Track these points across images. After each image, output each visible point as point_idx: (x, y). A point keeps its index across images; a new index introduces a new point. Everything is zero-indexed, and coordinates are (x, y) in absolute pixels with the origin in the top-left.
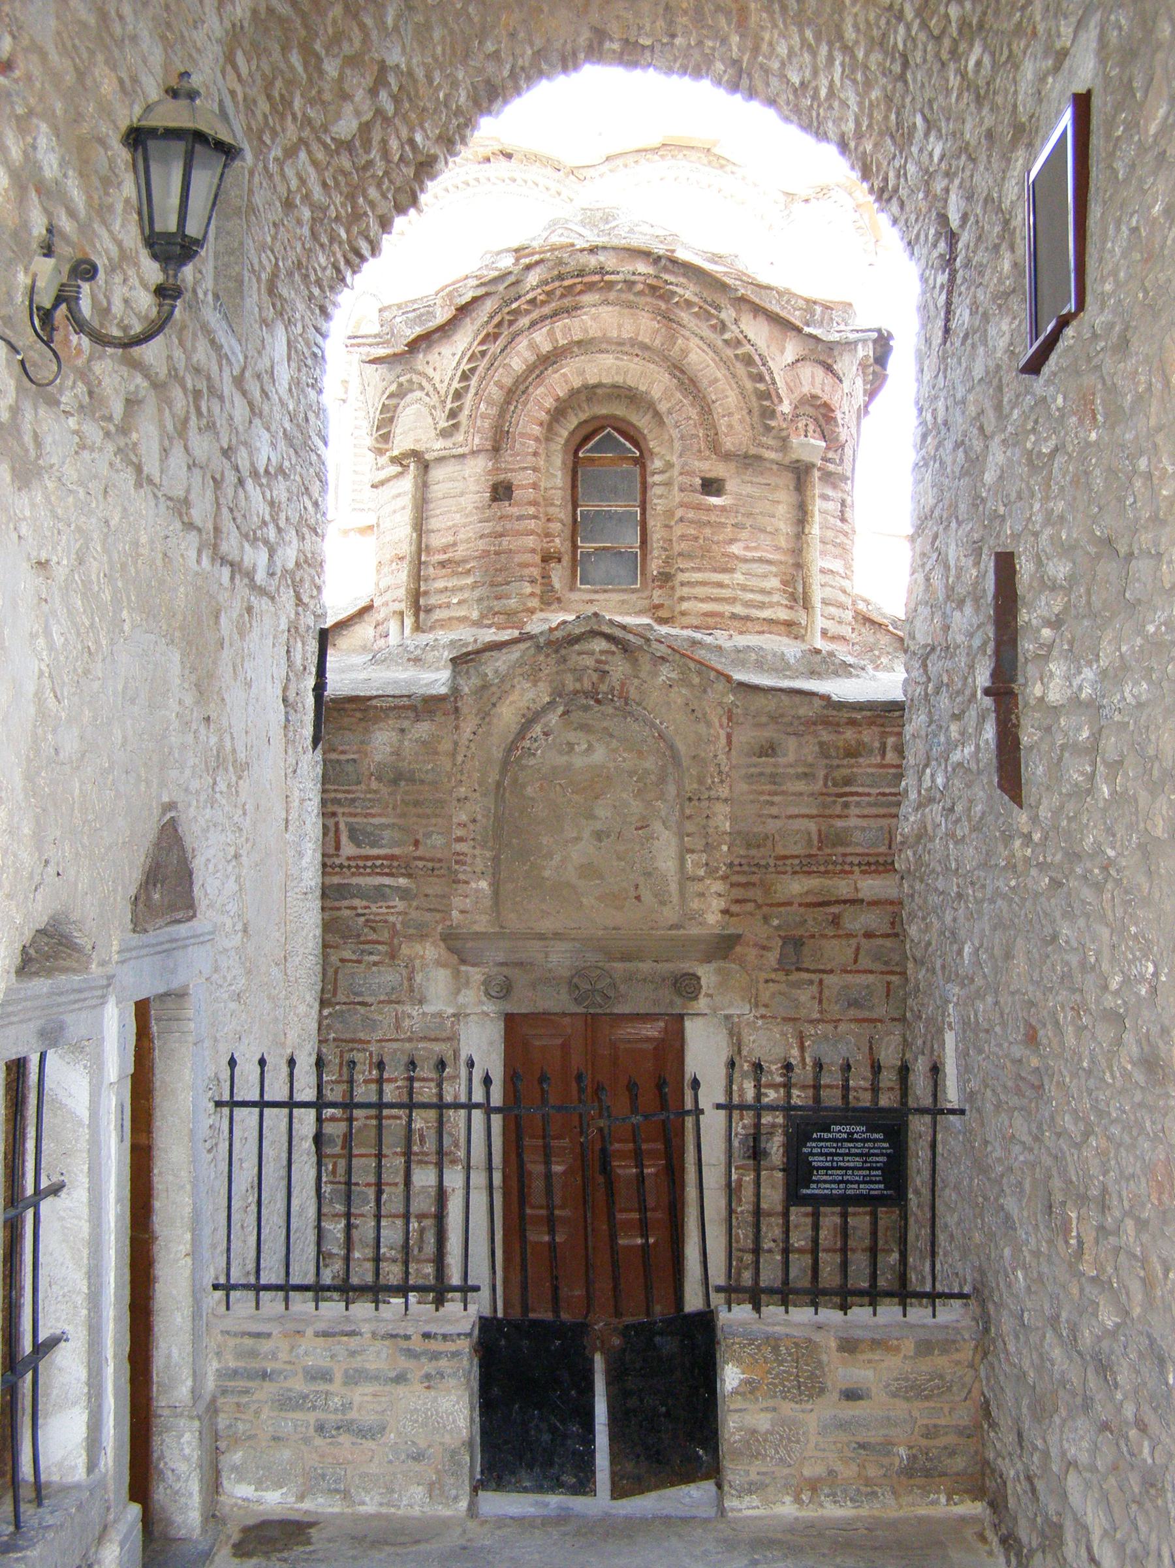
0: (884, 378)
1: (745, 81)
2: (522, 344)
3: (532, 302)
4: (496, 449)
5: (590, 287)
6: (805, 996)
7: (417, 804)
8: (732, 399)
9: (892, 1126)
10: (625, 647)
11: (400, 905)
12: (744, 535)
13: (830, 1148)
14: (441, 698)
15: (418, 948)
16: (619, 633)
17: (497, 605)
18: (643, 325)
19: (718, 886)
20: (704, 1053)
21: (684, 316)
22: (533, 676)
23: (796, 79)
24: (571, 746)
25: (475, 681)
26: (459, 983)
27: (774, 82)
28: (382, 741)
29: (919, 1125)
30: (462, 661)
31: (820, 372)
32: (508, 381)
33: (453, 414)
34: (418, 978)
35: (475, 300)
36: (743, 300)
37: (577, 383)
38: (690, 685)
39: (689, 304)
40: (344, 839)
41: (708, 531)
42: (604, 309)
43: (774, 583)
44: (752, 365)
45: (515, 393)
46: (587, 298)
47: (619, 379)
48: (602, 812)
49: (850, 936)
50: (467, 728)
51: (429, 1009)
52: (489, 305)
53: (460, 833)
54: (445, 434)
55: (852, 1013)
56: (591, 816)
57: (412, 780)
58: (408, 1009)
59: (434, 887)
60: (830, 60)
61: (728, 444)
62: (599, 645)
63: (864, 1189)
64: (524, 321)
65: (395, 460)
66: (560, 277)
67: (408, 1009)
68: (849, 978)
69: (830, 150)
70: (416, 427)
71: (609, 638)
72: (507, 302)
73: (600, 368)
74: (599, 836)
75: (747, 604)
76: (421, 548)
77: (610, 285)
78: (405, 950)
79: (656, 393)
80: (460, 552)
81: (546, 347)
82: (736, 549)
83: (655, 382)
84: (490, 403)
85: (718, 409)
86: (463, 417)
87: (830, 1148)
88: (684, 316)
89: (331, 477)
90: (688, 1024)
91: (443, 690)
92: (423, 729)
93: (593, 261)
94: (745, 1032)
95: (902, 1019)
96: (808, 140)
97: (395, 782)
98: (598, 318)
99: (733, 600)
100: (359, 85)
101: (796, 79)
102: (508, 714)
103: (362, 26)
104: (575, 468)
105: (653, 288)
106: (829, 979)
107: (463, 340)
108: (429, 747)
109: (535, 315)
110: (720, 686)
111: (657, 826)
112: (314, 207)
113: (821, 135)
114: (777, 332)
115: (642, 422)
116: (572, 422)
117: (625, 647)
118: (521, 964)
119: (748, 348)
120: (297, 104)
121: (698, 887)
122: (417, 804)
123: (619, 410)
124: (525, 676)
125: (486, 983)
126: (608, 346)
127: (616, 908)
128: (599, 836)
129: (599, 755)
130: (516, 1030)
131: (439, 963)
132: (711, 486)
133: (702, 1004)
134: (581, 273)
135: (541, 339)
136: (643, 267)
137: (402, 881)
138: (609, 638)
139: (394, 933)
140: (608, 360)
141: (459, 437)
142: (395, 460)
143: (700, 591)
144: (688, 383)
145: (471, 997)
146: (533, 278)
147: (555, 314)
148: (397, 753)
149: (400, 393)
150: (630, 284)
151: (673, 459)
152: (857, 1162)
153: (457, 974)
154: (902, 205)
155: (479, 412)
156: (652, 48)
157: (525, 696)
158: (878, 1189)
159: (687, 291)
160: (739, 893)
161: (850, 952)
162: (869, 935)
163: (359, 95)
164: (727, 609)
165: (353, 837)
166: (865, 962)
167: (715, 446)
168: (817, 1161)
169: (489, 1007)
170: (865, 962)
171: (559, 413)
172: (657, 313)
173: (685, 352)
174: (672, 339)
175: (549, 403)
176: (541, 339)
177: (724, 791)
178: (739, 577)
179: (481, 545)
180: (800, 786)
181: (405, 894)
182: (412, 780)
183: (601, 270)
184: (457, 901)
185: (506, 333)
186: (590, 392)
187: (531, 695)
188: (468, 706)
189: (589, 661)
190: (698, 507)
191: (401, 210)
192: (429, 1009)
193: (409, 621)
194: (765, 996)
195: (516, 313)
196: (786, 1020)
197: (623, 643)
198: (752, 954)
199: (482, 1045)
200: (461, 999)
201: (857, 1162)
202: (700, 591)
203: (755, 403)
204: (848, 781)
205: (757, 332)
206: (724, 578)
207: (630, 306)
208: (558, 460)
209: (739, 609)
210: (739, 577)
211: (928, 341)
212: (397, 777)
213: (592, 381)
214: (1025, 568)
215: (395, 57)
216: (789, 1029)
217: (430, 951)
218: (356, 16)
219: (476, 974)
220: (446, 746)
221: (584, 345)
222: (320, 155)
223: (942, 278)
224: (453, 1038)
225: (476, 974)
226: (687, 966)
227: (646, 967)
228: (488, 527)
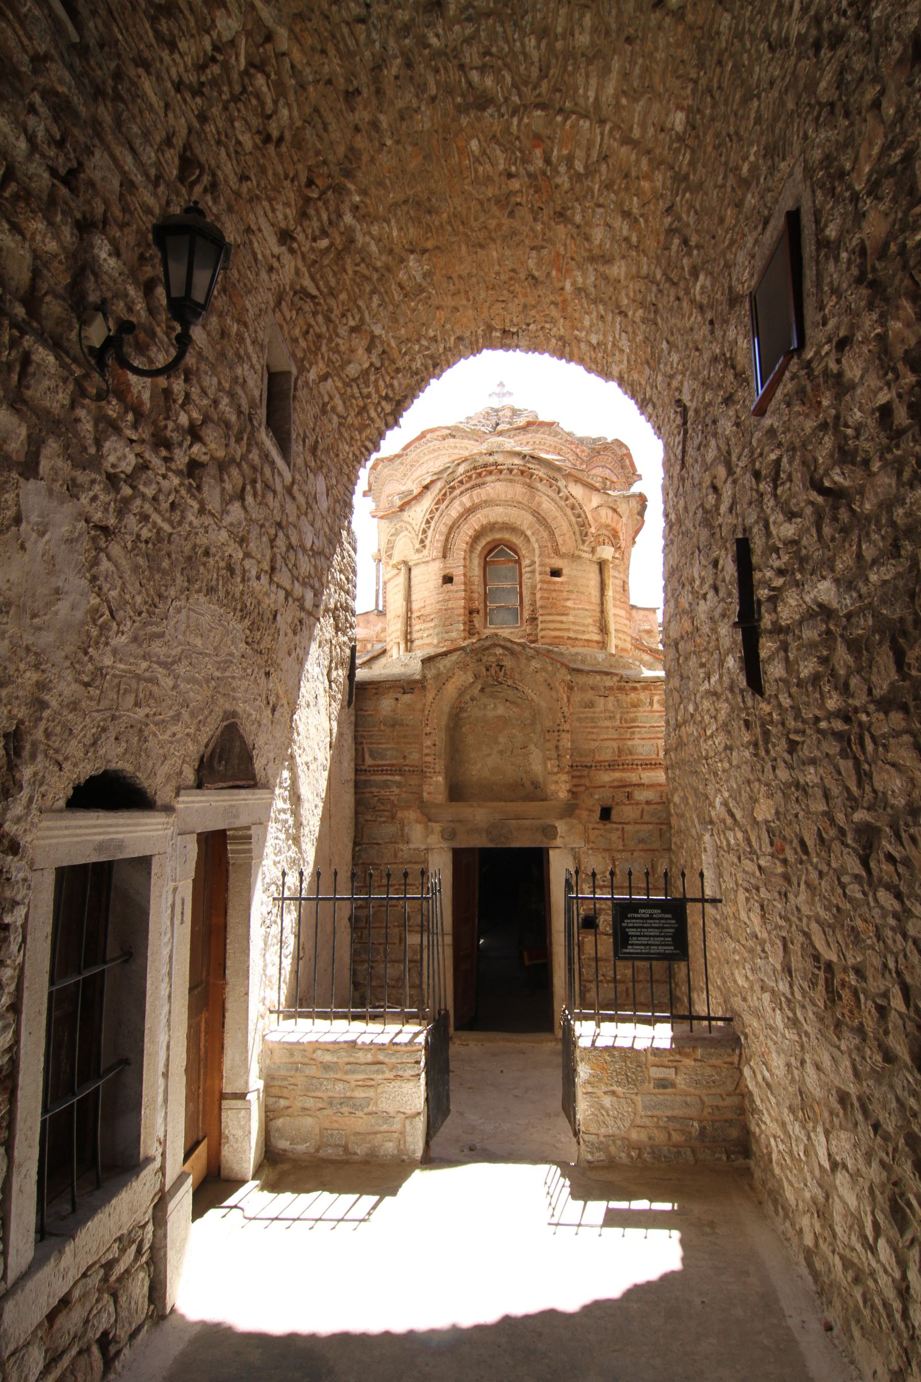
0: (643, 522)
1: (567, 349)
2: (456, 503)
3: (461, 482)
4: (444, 557)
5: (490, 473)
6: (614, 836)
7: (405, 737)
8: (565, 526)
9: (676, 909)
10: (512, 653)
11: (395, 790)
12: (574, 596)
13: (638, 923)
14: (416, 681)
15: (406, 813)
16: (509, 645)
17: (446, 636)
18: (518, 491)
19: (565, 777)
20: (559, 866)
21: (539, 485)
22: (464, 667)
23: (594, 342)
24: (485, 706)
25: (434, 671)
26: (428, 832)
27: (583, 345)
28: (386, 705)
29: (693, 910)
30: (427, 661)
31: (610, 513)
32: (450, 523)
33: (422, 541)
34: (406, 829)
35: (432, 482)
36: (569, 475)
37: (485, 522)
38: (546, 671)
39: (541, 480)
40: (367, 756)
41: (554, 595)
42: (498, 484)
43: (590, 621)
44: (574, 506)
45: (453, 528)
46: (489, 479)
47: (506, 519)
48: (502, 740)
49: (638, 804)
50: (430, 696)
51: (412, 846)
52: (439, 485)
53: (426, 751)
54: (418, 551)
55: (641, 846)
56: (497, 743)
57: (402, 725)
58: (401, 846)
59: (414, 781)
60: (613, 322)
61: (563, 550)
62: (499, 651)
63: (661, 949)
64: (457, 492)
65: (394, 566)
66: (475, 468)
67: (401, 846)
68: (638, 827)
69: (613, 385)
70: (405, 548)
71: (503, 647)
72: (448, 483)
73: (497, 514)
74: (501, 753)
75: (576, 631)
76: (409, 610)
77: (501, 472)
78: (399, 815)
79: (524, 527)
80: (428, 610)
81: (468, 504)
82: (569, 604)
83: (524, 520)
84: (441, 534)
85: (557, 532)
86: (427, 542)
87: (638, 923)
88: (539, 485)
89: (358, 569)
90: (551, 852)
91: (418, 677)
92: (407, 698)
93: (491, 459)
94: (583, 857)
95: (669, 849)
96: (599, 381)
97: (393, 726)
98: (494, 488)
99: (568, 630)
100: (360, 344)
101: (594, 342)
102: (451, 689)
103: (359, 308)
104: (486, 565)
105: (522, 472)
106: (627, 827)
107: (427, 502)
108: (410, 707)
109: (463, 488)
110: (564, 671)
111: (532, 747)
112: (339, 416)
113: (606, 375)
114: (587, 491)
115: (517, 540)
116: (483, 542)
117: (512, 653)
118: (460, 821)
119: (571, 500)
120: (324, 349)
121: (555, 778)
122: (405, 737)
123: (507, 536)
124: (460, 669)
125: (442, 832)
126: (501, 502)
127: (201, 213)
128: (501, 753)
129: (501, 711)
130: (458, 855)
131: (417, 821)
132: (556, 573)
133: (558, 842)
134: (485, 466)
135: (466, 500)
136: (517, 461)
137: (397, 778)
138: (503, 647)
139: (394, 805)
140: (500, 509)
141: (426, 552)
142: (394, 566)
143: (552, 626)
144: (541, 519)
145: (434, 840)
146: (461, 469)
147: (473, 487)
148: (394, 711)
149: (396, 534)
150: (511, 471)
151: (534, 559)
152: (656, 932)
153: (427, 827)
154: (654, 407)
155: (435, 539)
156: (517, 333)
157: (462, 678)
158: (669, 949)
159: (541, 472)
160: (576, 781)
161: (638, 813)
162: (648, 803)
163: (360, 351)
164: (566, 634)
165: (372, 756)
166: (646, 818)
167: (557, 552)
168: (631, 932)
169: (444, 845)
170: (646, 818)
171: (476, 538)
172: (525, 484)
173: (539, 504)
174: (533, 497)
175: (471, 532)
176: (466, 500)
177: (567, 727)
178: (571, 618)
179: (438, 606)
180: (608, 723)
181: (399, 785)
182: (402, 725)
183: (496, 464)
184: (426, 787)
185: (448, 498)
186: (491, 527)
187: (463, 678)
188: (430, 684)
189: (493, 659)
190: (549, 582)
191: (389, 427)
192: (412, 846)
193: (402, 646)
194: (592, 838)
195: (453, 488)
196: (605, 850)
197: (509, 648)
198: (585, 814)
199: (440, 867)
200: (429, 840)
201: (656, 932)
202: (552, 626)
203: (577, 528)
204: (633, 720)
205: (577, 491)
206: (563, 618)
207: (511, 481)
208: (476, 561)
209: (572, 635)
210: (571, 618)
211: (671, 477)
212: (394, 723)
213: (492, 520)
214: (758, 543)
215: (378, 330)
216: (607, 855)
217: (412, 815)
218: (355, 302)
219: (437, 827)
220: (419, 706)
221: (487, 503)
222: (340, 385)
223: (679, 438)
224: (426, 861)
225: (437, 827)
226: (549, 821)
227: (527, 822)
228: (441, 597)
